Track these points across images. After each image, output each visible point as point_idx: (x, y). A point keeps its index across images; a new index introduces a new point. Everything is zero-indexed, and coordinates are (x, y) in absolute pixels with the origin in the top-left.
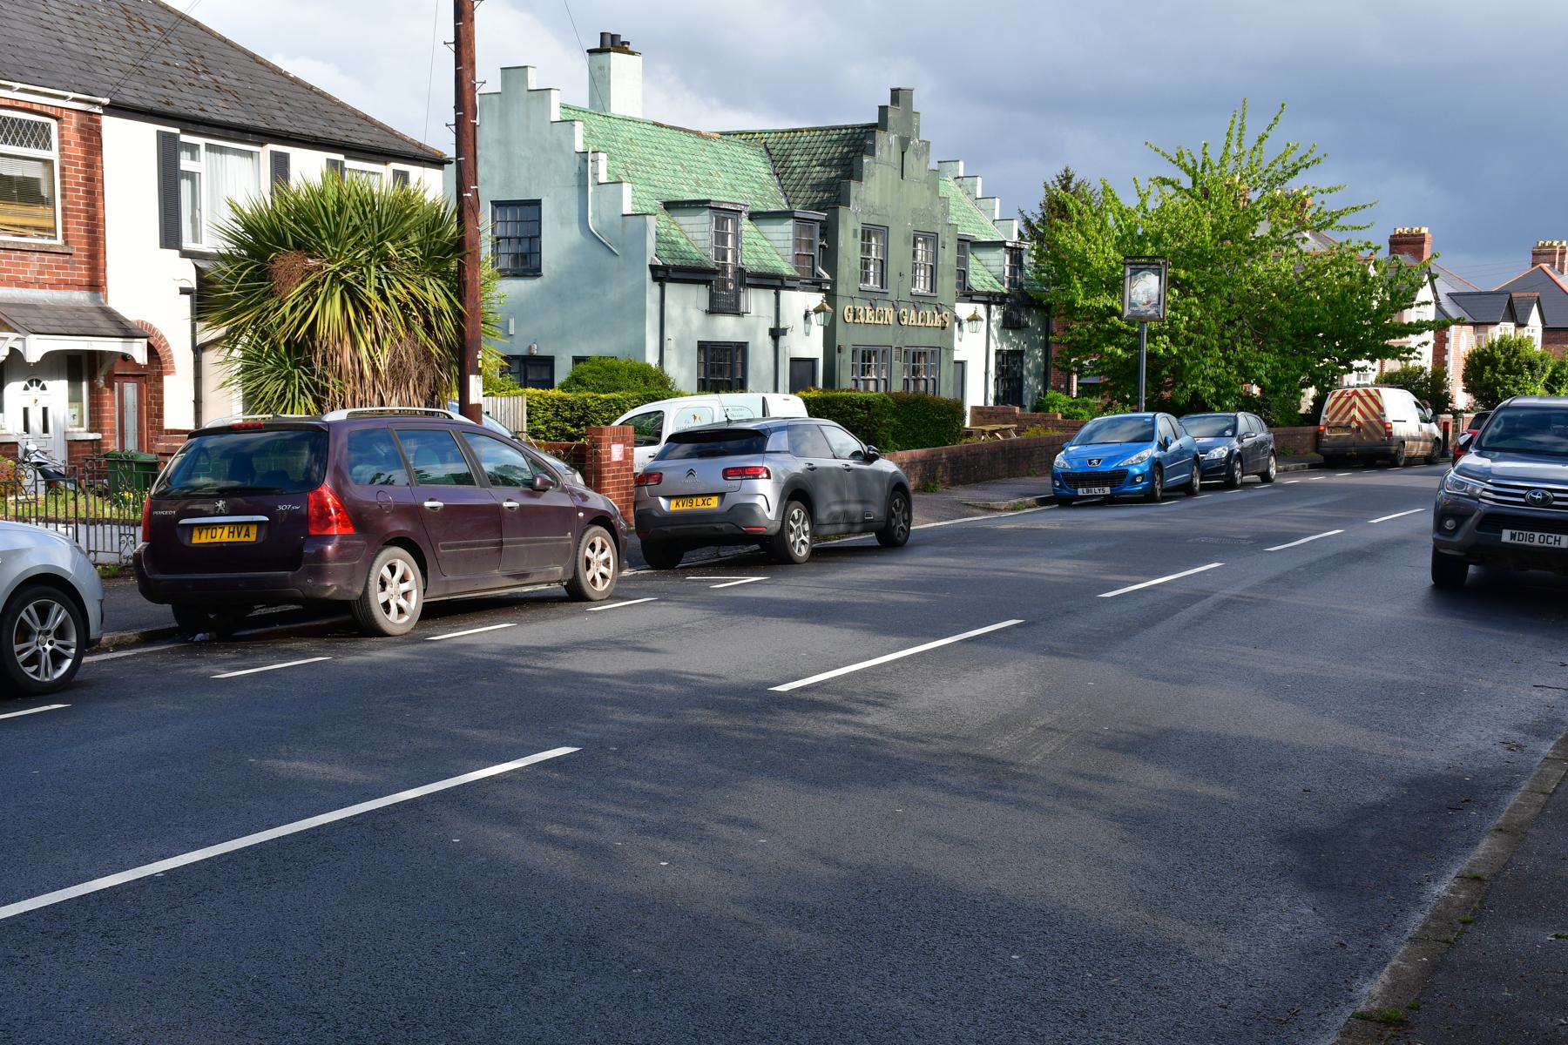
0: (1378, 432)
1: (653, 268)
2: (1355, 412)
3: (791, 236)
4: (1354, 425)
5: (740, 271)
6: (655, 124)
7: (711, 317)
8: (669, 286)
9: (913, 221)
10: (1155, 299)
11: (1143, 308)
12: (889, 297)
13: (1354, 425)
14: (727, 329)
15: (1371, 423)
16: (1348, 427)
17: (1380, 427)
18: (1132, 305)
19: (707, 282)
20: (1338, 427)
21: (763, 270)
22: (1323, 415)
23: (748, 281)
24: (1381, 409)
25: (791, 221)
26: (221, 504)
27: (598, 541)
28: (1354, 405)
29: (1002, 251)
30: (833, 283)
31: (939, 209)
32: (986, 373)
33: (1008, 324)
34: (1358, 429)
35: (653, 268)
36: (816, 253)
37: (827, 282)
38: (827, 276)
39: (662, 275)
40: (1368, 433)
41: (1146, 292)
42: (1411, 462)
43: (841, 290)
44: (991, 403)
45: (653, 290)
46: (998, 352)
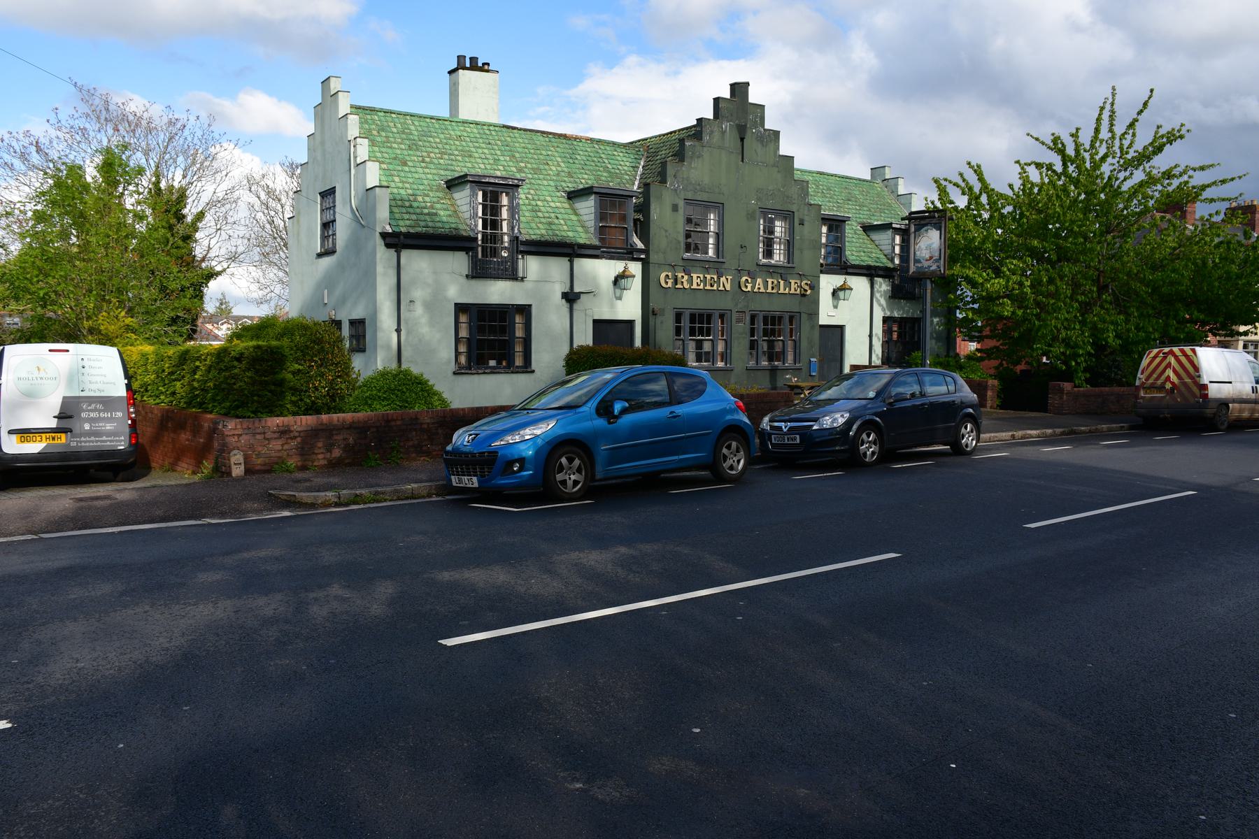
0: (1194, 395)
1: (384, 235)
2: (1170, 372)
3: (593, 210)
4: (1168, 386)
5: (515, 240)
6: (504, 126)
7: (474, 282)
8: (405, 254)
9: (758, 199)
10: (937, 254)
11: (926, 264)
12: (796, 271)
13: (1168, 386)
14: (497, 292)
15: (1185, 384)
16: (1162, 387)
17: (1195, 389)
18: (917, 261)
19: (466, 250)
20: (1153, 387)
21: (556, 239)
22: (1139, 375)
23: (522, 248)
24: (1197, 369)
25: (593, 197)
26: (87, 426)
27: (734, 444)
28: (1169, 365)
29: (890, 232)
30: (646, 251)
31: (794, 191)
32: (871, 336)
33: (896, 294)
34: (1172, 390)
35: (384, 235)
36: (630, 225)
37: (641, 251)
38: (640, 245)
39: (397, 241)
40: (1181, 394)
41: (929, 247)
42: (571, 497)
43: (654, 258)
44: (877, 361)
45: (384, 256)
46: (886, 320)
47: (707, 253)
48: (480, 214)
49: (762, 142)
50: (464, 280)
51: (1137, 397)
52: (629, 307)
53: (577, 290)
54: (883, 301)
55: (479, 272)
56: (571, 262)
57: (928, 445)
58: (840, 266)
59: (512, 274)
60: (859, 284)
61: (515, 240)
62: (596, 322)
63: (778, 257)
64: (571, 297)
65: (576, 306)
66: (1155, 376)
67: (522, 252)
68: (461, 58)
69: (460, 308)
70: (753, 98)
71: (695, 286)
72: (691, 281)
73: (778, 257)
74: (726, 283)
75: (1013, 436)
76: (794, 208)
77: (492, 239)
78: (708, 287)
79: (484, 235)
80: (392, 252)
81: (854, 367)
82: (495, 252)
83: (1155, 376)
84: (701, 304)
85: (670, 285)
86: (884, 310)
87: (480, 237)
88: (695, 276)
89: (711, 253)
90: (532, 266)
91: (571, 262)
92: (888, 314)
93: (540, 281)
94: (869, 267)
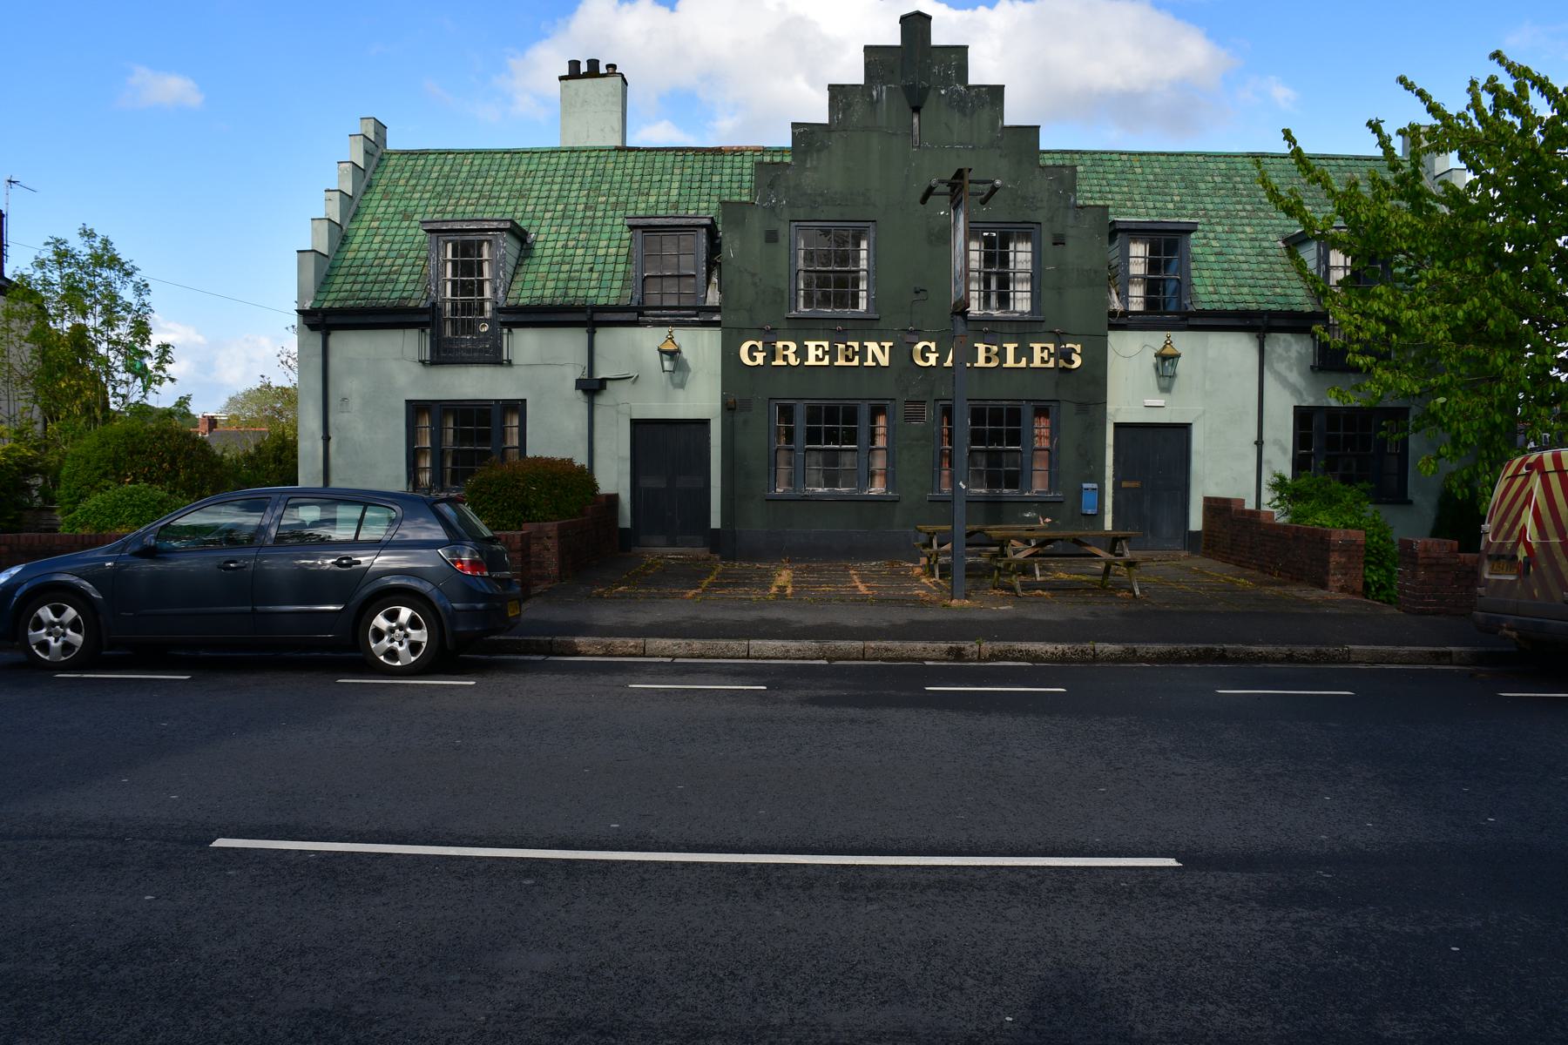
13: (1522, 553)
14: (470, 384)
46: (1303, 416)
47: (856, 305)
48: (449, 275)
49: (962, 111)
50: (418, 369)
51: (1473, 575)
52: (701, 398)
53: (600, 374)
54: (1294, 377)
55: (442, 356)
56: (591, 335)
57: (504, 653)
58: (1168, 310)
59: (495, 358)
60: (1236, 349)
61: (498, 310)
62: (636, 424)
63: (1022, 303)
64: (592, 387)
65: (600, 400)
66: (1507, 525)
67: (504, 324)
68: (574, 65)
69: (416, 409)
70: (938, 38)
71: (811, 361)
72: (802, 352)
73: (1022, 303)
74: (878, 352)
75: (958, 654)
76: (1040, 216)
77: (469, 308)
78: (841, 362)
79: (454, 303)
80: (317, 338)
81: (1215, 507)
82: (470, 327)
83: (1507, 525)
84: (825, 392)
85: (760, 361)
86: (1295, 390)
87: (448, 306)
88: (811, 345)
89: (863, 305)
90: (525, 344)
91: (591, 335)
92: (1309, 401)
93: (538, 368)
94: (1258, 314)
